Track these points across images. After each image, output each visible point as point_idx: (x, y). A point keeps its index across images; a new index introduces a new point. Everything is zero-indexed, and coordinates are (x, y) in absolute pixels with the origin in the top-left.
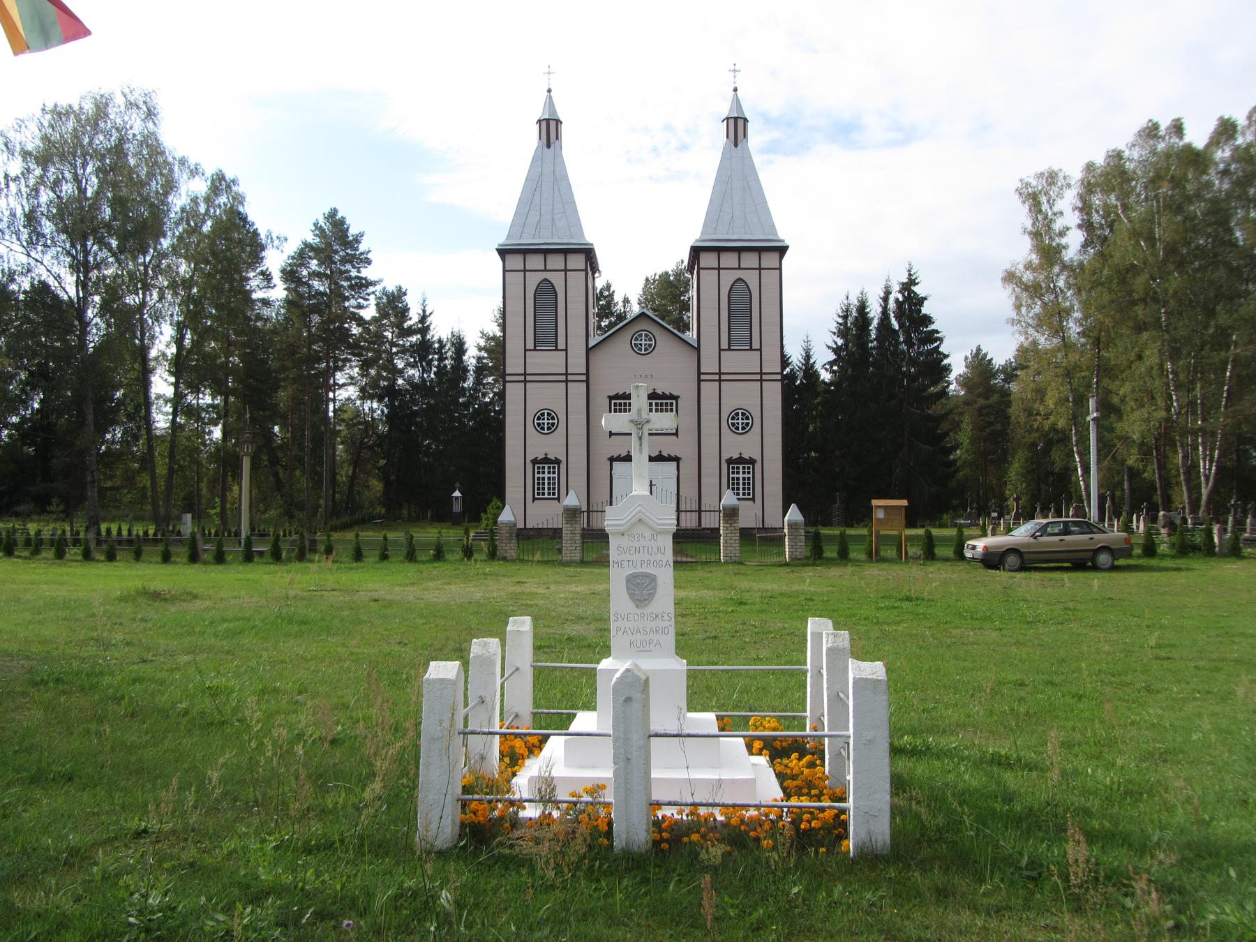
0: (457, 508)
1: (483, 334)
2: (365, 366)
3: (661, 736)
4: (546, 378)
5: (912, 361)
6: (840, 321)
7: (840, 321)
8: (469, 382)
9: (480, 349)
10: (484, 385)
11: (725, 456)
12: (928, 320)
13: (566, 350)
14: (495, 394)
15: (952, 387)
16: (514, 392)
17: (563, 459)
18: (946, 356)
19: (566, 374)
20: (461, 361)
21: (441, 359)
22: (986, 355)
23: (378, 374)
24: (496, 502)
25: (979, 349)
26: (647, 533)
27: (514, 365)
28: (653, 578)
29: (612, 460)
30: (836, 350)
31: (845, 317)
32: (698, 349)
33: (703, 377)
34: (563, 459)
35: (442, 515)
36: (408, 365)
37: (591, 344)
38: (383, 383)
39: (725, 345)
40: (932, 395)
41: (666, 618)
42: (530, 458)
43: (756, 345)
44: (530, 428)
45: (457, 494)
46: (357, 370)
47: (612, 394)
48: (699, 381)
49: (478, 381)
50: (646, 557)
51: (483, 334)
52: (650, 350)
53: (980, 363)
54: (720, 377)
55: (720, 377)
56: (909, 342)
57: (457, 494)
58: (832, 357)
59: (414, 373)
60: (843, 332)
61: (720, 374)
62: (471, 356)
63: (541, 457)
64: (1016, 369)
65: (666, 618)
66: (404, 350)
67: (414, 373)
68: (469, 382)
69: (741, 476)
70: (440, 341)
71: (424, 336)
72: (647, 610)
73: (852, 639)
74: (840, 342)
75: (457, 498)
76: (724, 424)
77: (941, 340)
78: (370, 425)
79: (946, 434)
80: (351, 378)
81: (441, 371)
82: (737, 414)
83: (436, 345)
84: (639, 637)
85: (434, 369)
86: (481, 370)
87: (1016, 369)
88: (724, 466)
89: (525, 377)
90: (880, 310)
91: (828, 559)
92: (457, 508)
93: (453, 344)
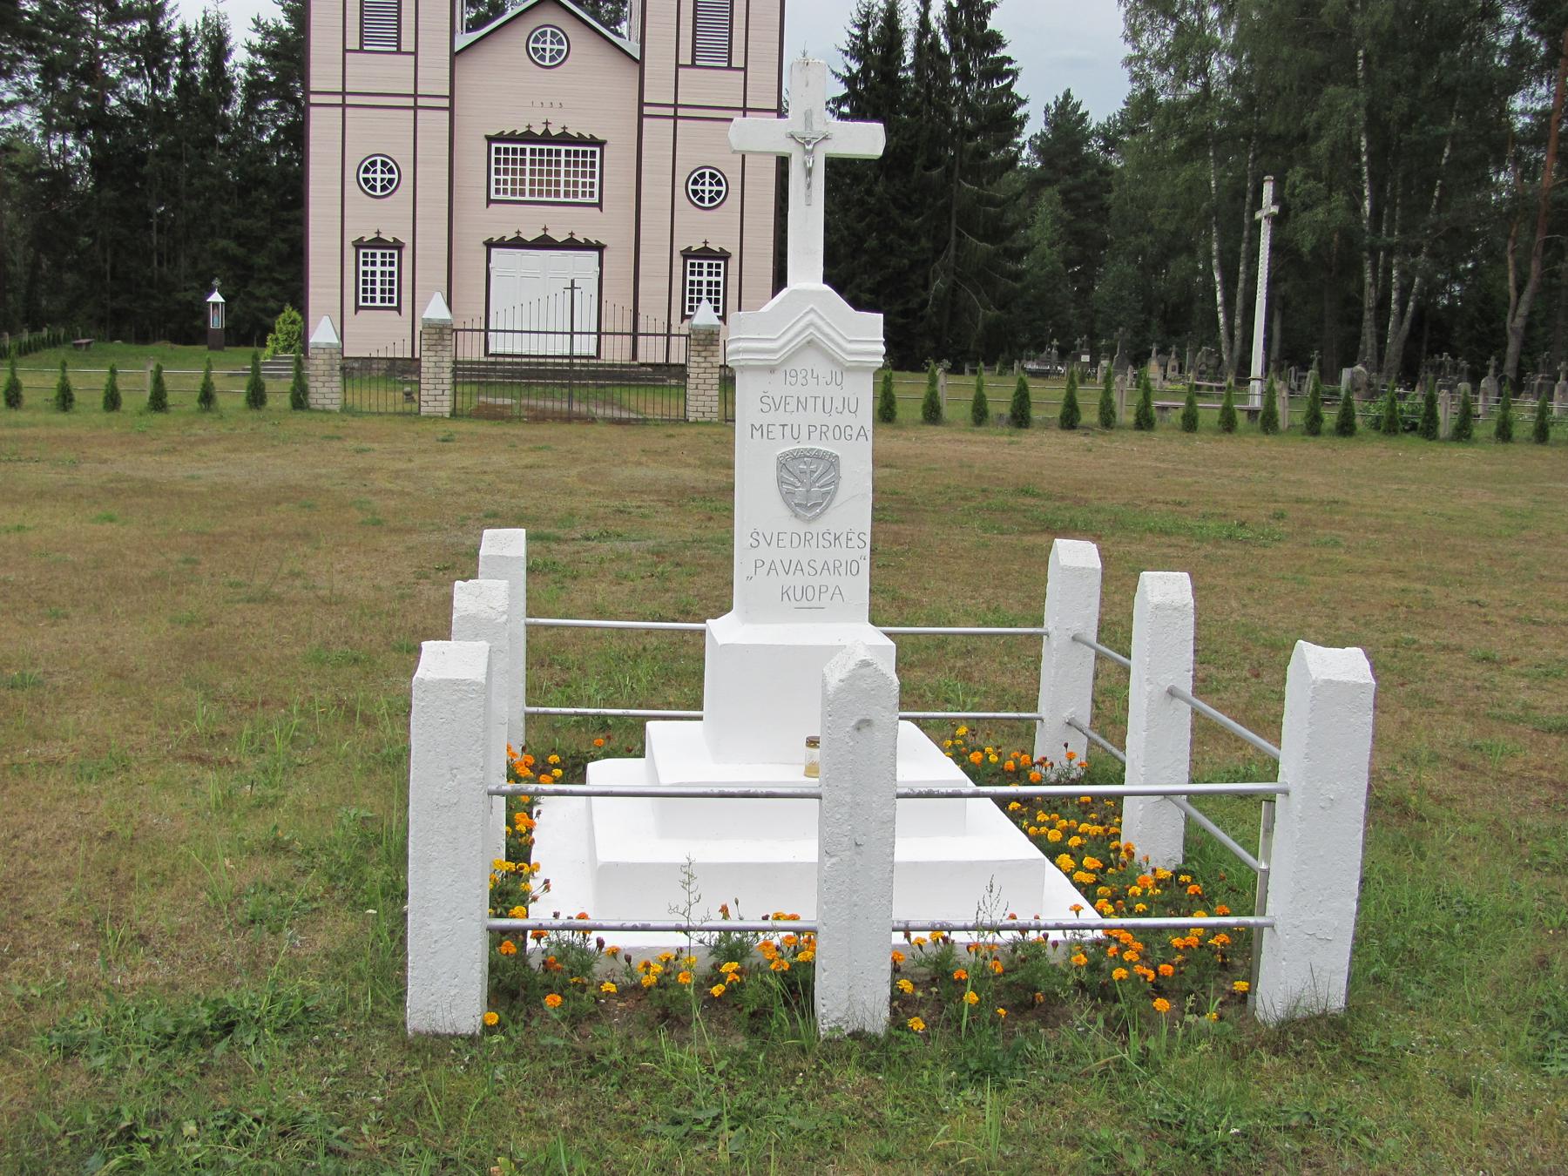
0: (216, 322)
1: (259, 25)
2: (50, 71)
3: (920, 795)
4: (379, 101)
5: (969, 108)
6: (857, 32)
7: (857, 32)
8: (235, 109)
9: (253, 50)
10: (260, 113)
11: (680, 246)
12: (995, 41)
13: (415, 54)
14: (280, 129)
15: (1024, 154)
16: (322, 125)
17: (408, 241)
18: (1022, 102)
19: (415, 96)
20: (222, 71)
21: (186, 66)
22: (1078, 106)
23: (74, 88)
24: (290, 312)
25: (1067, 95)
26: (823, 369)
27: (323, 73)
28: (832, 462)
29: (490, 245)
30: (850, 81)
31: (864, 27)
32: (640, 63)
33: (647, 110)
34: (408, 241)
35: (186, 329)
36: (127, 72)
37: (457, 49)
38: (84, 105)
39: (686, 59)
40: (996, 163)
41: (855, 542)
42: (351, 238)
43: (738, 61)
44: (352, 187)
45: (216, 297)
46: (34, 78)
47: (493, 133)
48: (641, 116)
49: (250, 106)
50: (818, 418)
51: (259, 25)
52: (559, 59)
53: (1065, 117)
54: (676, 112)
55: (676, 112)
56: (965, 75)
57: (216, 297)
58: (842, 90)
59: (138, 87)
60: (859, 50)
61: (676, 106)
62: (238, 60)
63: (370, 236)
64: (1121, 132)
65: (855, 542)
66: (117, 45)
67: (138, 87)
68: (235, 109)
69: (705, 278)
70: (184, 33)
71: (153, 24)
72: (818, 527)
73: (1195, 589)
74: (856, 67)
75: (216, 305)
76: (680, 191)
77: (1015, 73)
78: (60, 180)
79: (1015, 227)
80: (26, 92)
81: (185, 86)
82: (702, 176)
83: (178, 41)
84: (798, 580)
85: (173, 83)
86: (256, 88)
87: (1121, 132)
88: (678, 261)
89: (343, 99)
90: (916, 17)
91: (1122, 427)
92: (216, 322)
93: (207, 39)
